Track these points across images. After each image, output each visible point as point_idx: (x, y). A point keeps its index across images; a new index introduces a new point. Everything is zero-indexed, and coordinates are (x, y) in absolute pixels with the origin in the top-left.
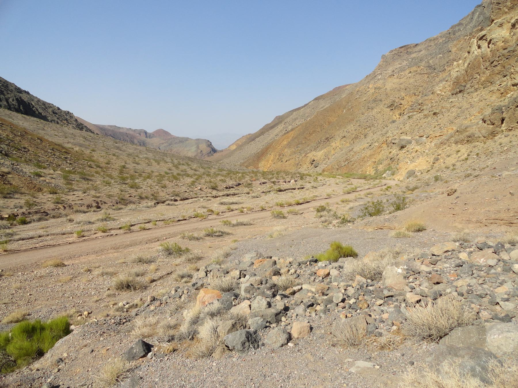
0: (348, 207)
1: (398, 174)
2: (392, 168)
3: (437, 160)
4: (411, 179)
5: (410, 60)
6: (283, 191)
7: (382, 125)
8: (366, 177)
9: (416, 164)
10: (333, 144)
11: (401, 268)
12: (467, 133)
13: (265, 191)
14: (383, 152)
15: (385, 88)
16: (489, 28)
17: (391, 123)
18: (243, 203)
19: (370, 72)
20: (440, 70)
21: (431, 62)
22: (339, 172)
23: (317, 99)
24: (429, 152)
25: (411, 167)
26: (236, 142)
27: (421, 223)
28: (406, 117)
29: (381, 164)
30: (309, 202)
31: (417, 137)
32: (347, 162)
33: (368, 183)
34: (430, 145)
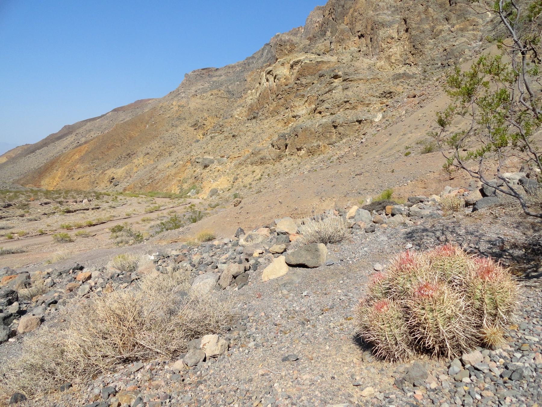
0: (150, 225)
1: (202, 193)
2: (196, 187)
3: (237, 179)
4: (214, 197)
5: (211, 82)
6: (73, 212)
7: (187, 144)
8: (171, 196)
9: (218, 183)
10: (136, 161)
11: (154, 255)
12: (260, 156)
13: (47, 212)
14: (187, 171)
15: (188, 107)
16: (274, 65)
17: (195, 142)
18: (13, 227)
19: (173, 89)
20: (238, 96)
21: (230, 87)
22: (142, 191)
23: (115, 110)
24: (230, 172)
25: (214, 185)
26: (6, 153)
27: (212, 233)
28: (209, 137)
29: (186, 182)
30: (105, 223)
31: (219, 157)
32: (151, 181)
33: (172, 202)
34: (230, 165)
